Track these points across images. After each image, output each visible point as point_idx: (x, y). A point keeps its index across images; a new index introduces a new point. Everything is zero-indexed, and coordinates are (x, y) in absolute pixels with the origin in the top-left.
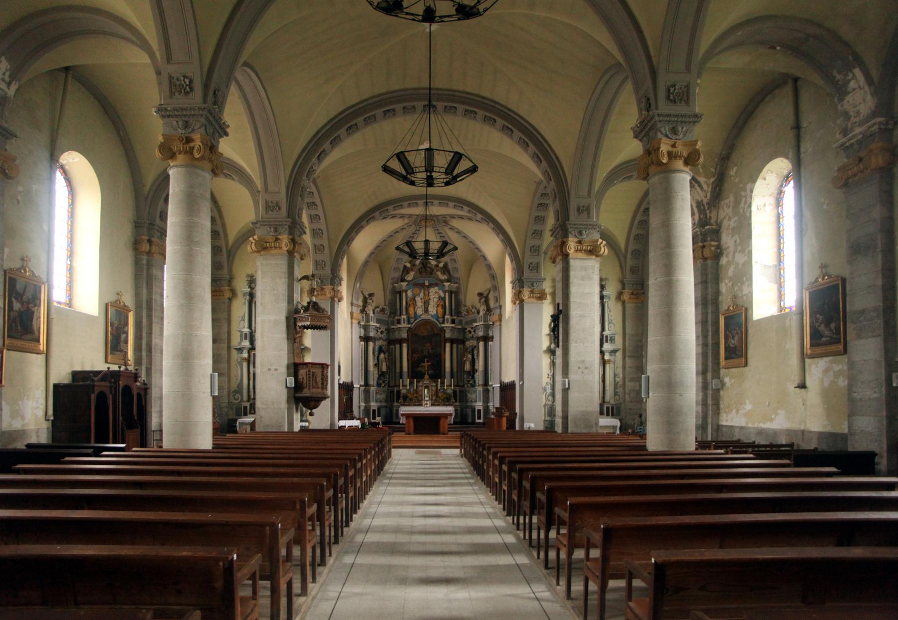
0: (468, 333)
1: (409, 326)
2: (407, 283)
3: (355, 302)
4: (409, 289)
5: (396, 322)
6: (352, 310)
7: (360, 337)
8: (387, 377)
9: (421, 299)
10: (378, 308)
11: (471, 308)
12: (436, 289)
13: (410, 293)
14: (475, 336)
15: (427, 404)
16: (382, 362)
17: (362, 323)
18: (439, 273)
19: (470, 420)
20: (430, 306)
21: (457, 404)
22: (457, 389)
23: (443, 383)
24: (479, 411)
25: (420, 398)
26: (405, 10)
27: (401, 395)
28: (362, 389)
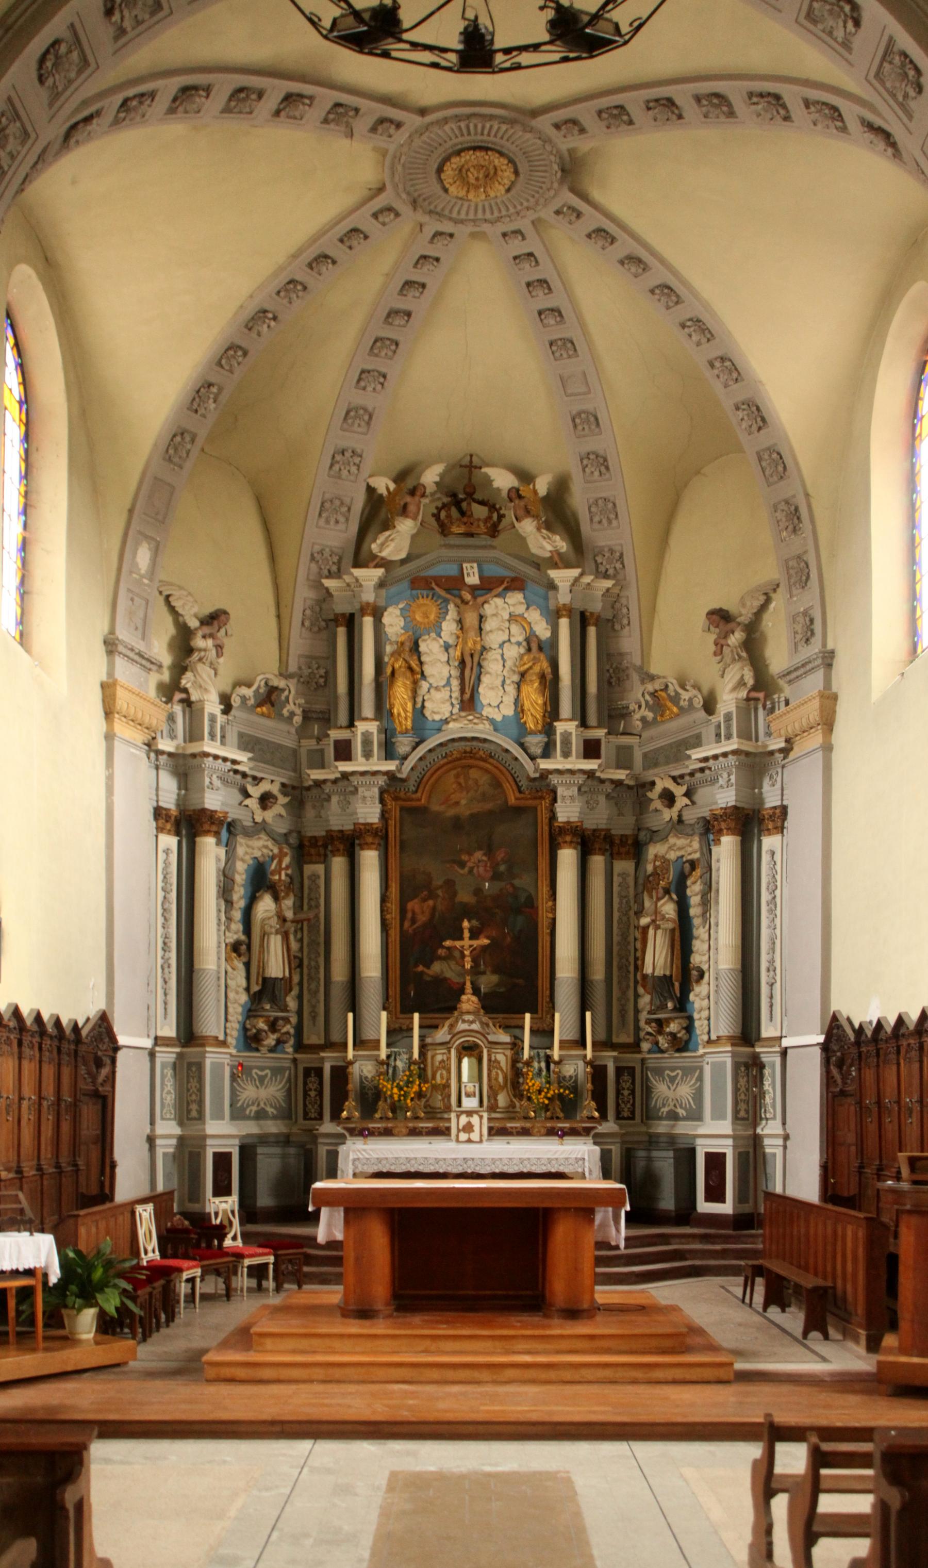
0: (657, 804)
1: (391, 766)
2: (380, 572)
3: (122, 634)
4: (391, 602)
5: (330, 752)
6: (111, 672)
7: (159, 813)
8: (292, 1004)
9: (447, 647)
10: (249, 686)
11: (674, 687)
12: (515, 599)
13: (393, 621)
14: (690, 816)
15: (469, 1128)
16: (264, 935)
17: (166, 745)
18: (528, 527)
19: (667, 1202)
20: (485, 679)
21: (609, 1126)
22: (609, 1059)
23: (544, 1033)
24: (715, 1161)
25: (437, 1101)
26: (405, 36)
27: (353, 1086)
28: (166, 1055)
